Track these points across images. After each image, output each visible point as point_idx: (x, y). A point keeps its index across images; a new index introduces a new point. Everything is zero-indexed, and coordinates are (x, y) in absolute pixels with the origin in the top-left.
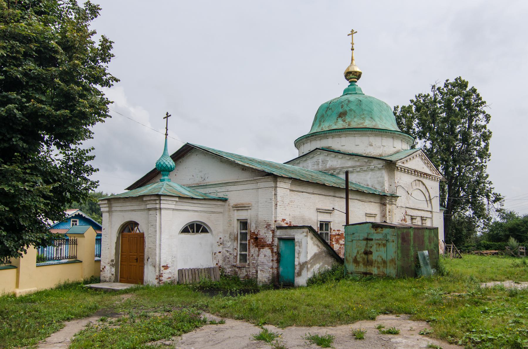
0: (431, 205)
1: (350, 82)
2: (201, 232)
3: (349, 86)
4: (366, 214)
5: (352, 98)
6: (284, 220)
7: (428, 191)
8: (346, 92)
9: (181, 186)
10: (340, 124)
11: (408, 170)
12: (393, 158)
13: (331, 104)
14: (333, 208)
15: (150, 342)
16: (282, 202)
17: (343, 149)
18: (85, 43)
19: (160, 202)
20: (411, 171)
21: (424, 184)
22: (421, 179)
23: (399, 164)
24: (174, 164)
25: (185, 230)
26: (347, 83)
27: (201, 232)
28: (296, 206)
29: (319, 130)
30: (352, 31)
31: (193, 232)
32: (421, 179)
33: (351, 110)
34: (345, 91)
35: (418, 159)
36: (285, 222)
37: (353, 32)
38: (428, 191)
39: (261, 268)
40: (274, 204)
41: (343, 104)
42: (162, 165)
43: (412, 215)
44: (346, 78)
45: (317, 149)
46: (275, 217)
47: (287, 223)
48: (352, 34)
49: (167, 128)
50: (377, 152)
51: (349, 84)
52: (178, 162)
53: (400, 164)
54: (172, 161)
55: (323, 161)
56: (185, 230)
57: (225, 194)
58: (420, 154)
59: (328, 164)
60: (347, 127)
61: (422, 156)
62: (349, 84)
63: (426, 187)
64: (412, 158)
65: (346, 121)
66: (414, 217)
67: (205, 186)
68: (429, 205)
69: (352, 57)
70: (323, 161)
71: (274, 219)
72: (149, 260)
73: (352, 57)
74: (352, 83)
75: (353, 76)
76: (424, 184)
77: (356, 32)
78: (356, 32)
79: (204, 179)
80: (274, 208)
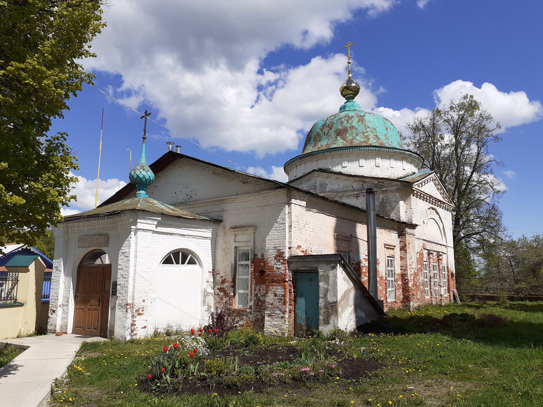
0: (446, 238)
1: (346, 99)
2: (187, 264)
3: (345, 103)
4: (385, 245)
6: (299, 247)
7: (442, 222)
8: (343, 109)
10: (340, 143)
11: (424, 195)
12: (408, 179)
13: (327, 121)
14: (351, 235)
15: (51, 276)
16: (297, 223)
18: (48, 25)
20: (427, 197)
21: (438, 213)
22: (436, 207)
23: (415, 186)
24: (153, 175)
25: (168, 261)
27: (187, 264)
28: (311, 230)
29: (314, 150)
31: (178, 263)
32: (436, 207)
33: (352, 127)
34: (341, 109)
35: (431, 184)
36: (301, 249)
38: (442, 222)
39: (269, 312)
40: (287, 226)
41: (343, 120)
42: (138, 176)
43: (429, 249)
44: (342, 94)
45: (314, 170)
46: (290, 243)
47: (303, 251)
49: (144, 130)
50: (385, 174)
52: (159, 174)
53: (416, 187)
54: (150, 171)
55: (321, 185)
56: (168, 261)
57: (219, 215)
59: (327, 188)
60: (348, 145)
61: (435, 180)
63: (440, 218)
65: (347, 139)
67: (136, 257)
68: (444, 237)
70: (321, 185)
71: (287, 245)
75: (351, 92)
76: (438, 213)
79: (191, 197)
80: (287, 230)
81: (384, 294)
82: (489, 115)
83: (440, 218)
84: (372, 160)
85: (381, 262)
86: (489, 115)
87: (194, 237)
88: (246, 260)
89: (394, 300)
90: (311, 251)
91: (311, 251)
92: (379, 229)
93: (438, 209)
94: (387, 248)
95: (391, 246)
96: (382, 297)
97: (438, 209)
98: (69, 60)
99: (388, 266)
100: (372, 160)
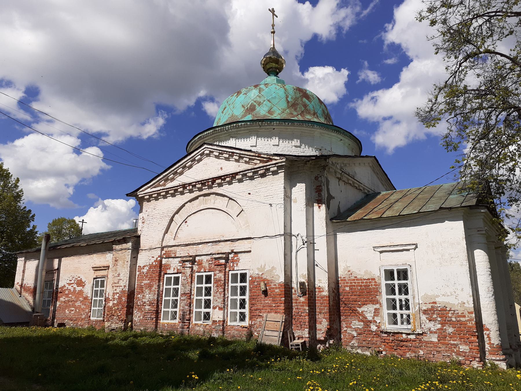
81: (86, 312)
82: (19, 186)
83: (177, 212)
84: (243, 140)
85: (87, 284)
86: (19, 186)
87: (296, 258)
88: (392, 280)
89: (102, 319)
90: (28, 284)
91: (28, 284)
92: (89, 256)
93: (215, 190)
94: (95, 270)
95: (101, 267)
96: (84, 314)
97: (215, 190)
98: (462, 41)
99: (97, 286)
100: (243, 140)
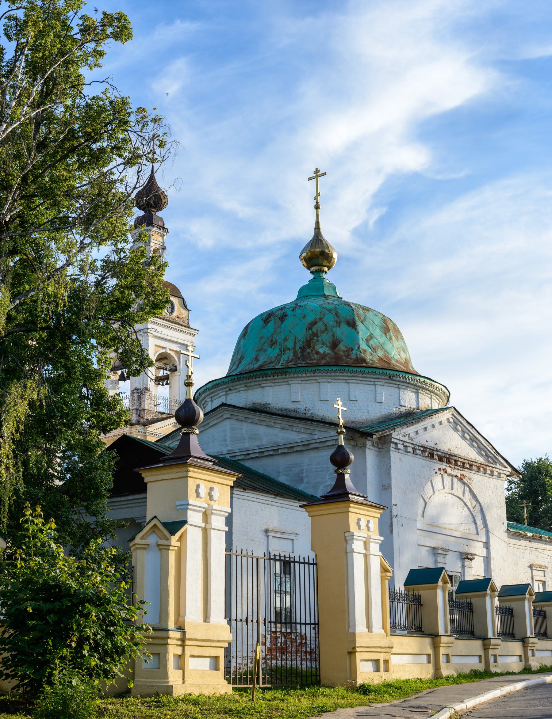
1: (312, 273)
5: (314, 303)
9: (148, 545)
17: (193, 476)
19: (273, 622)
26: (306, 276)
30: (317, 171)
37: (318, 174)
48: (317, 177)
51: (312, 276)
58: (451, 420)
62: (312, 276)
64: (437, 425)
66: (440, 551)
69: (317, 223)
72: (213, 493)
73: (317, 223)
74: (318, 273)
77: (324, 174)
78: (324, 174)
